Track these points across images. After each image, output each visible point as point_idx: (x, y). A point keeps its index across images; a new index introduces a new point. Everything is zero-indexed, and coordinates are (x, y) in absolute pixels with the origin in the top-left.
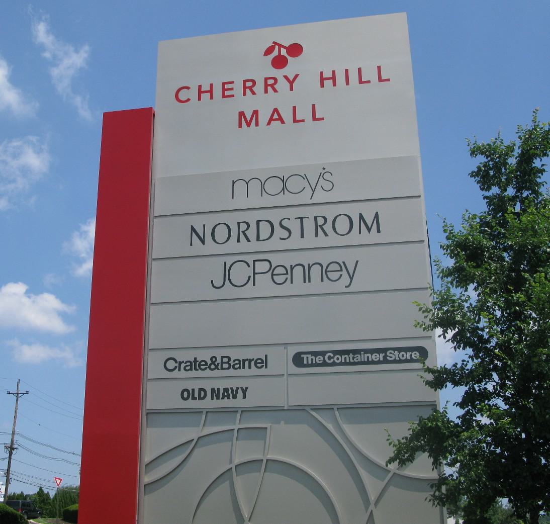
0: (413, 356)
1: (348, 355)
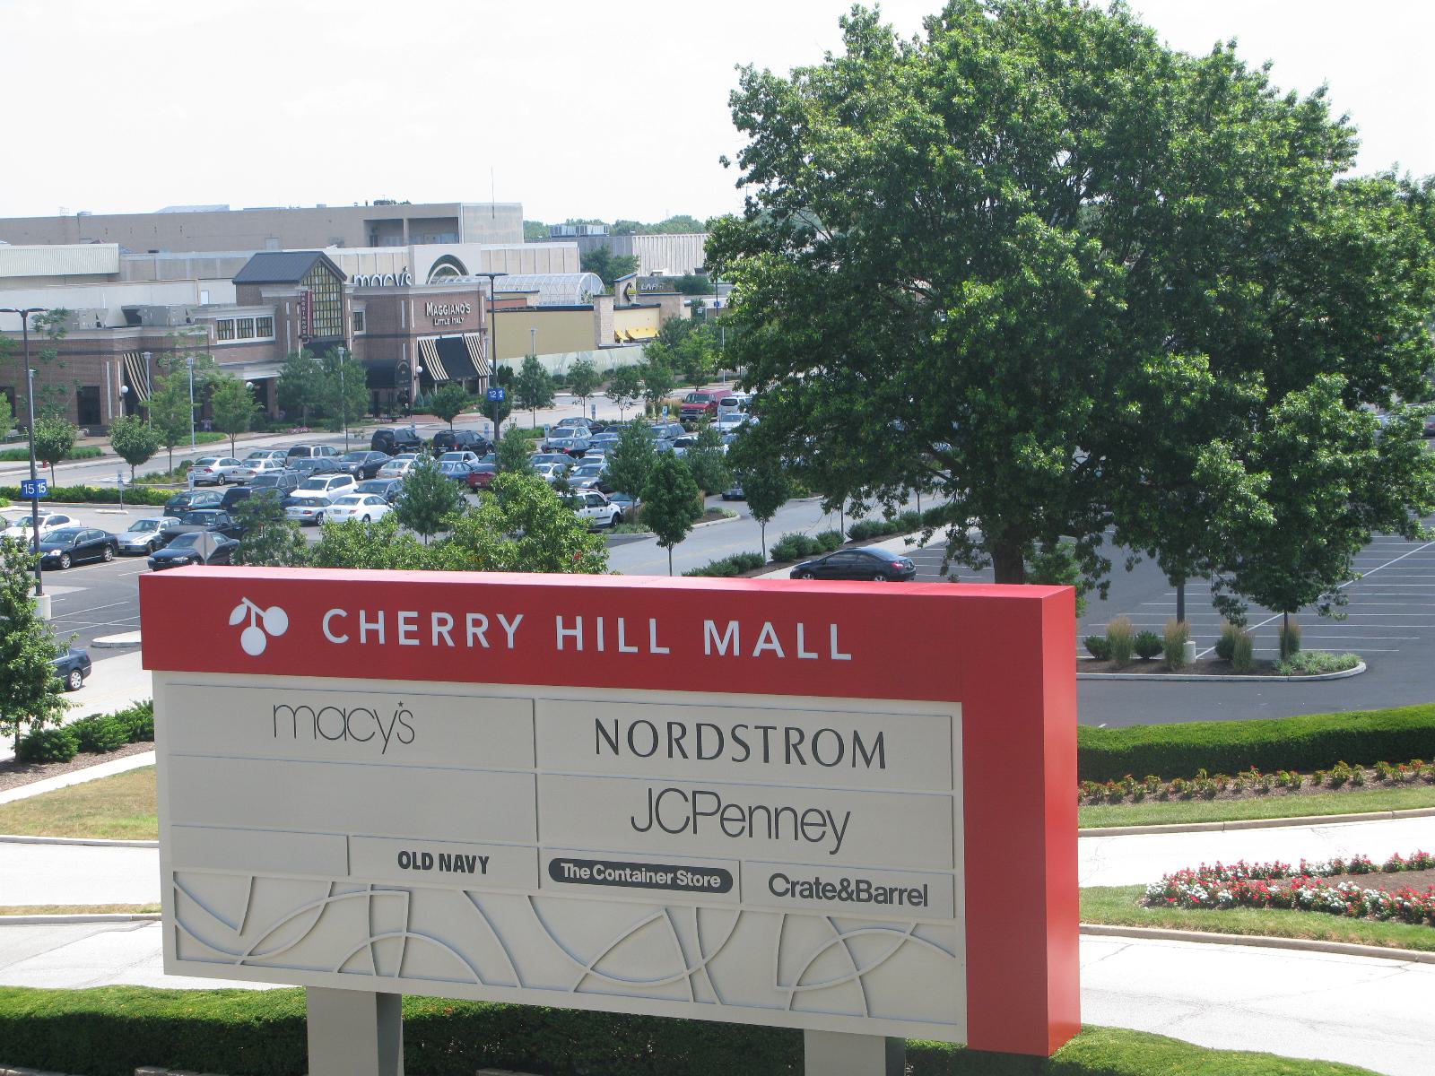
0: (712, 882)
1: (624, 870)
